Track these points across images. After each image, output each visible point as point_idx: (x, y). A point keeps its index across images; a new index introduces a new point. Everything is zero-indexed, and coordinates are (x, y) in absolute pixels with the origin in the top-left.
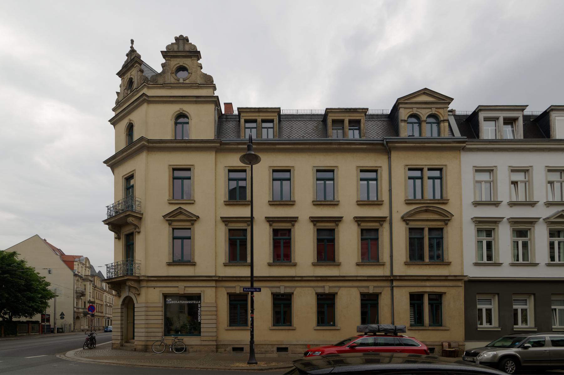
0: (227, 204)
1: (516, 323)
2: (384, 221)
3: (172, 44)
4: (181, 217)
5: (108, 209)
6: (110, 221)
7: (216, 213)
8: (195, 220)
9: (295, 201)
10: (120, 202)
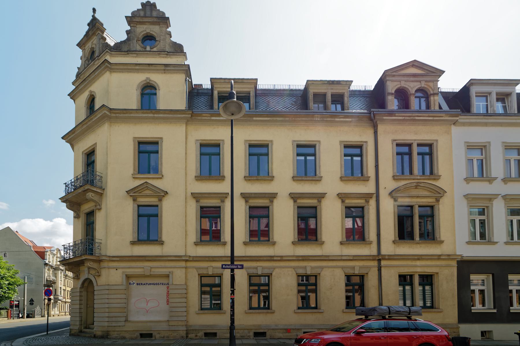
0: (199, 178)
1: (512, 305)
2: (371, 198)
3: (138, 10)
4: (148, 192)
5: (66, 186)
6: (67, 198)
7: (186, 189)
8: (163, 196)
10: (79, 177)
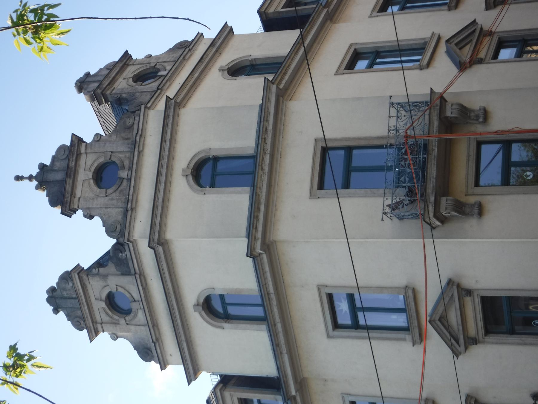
4: (454, 317)
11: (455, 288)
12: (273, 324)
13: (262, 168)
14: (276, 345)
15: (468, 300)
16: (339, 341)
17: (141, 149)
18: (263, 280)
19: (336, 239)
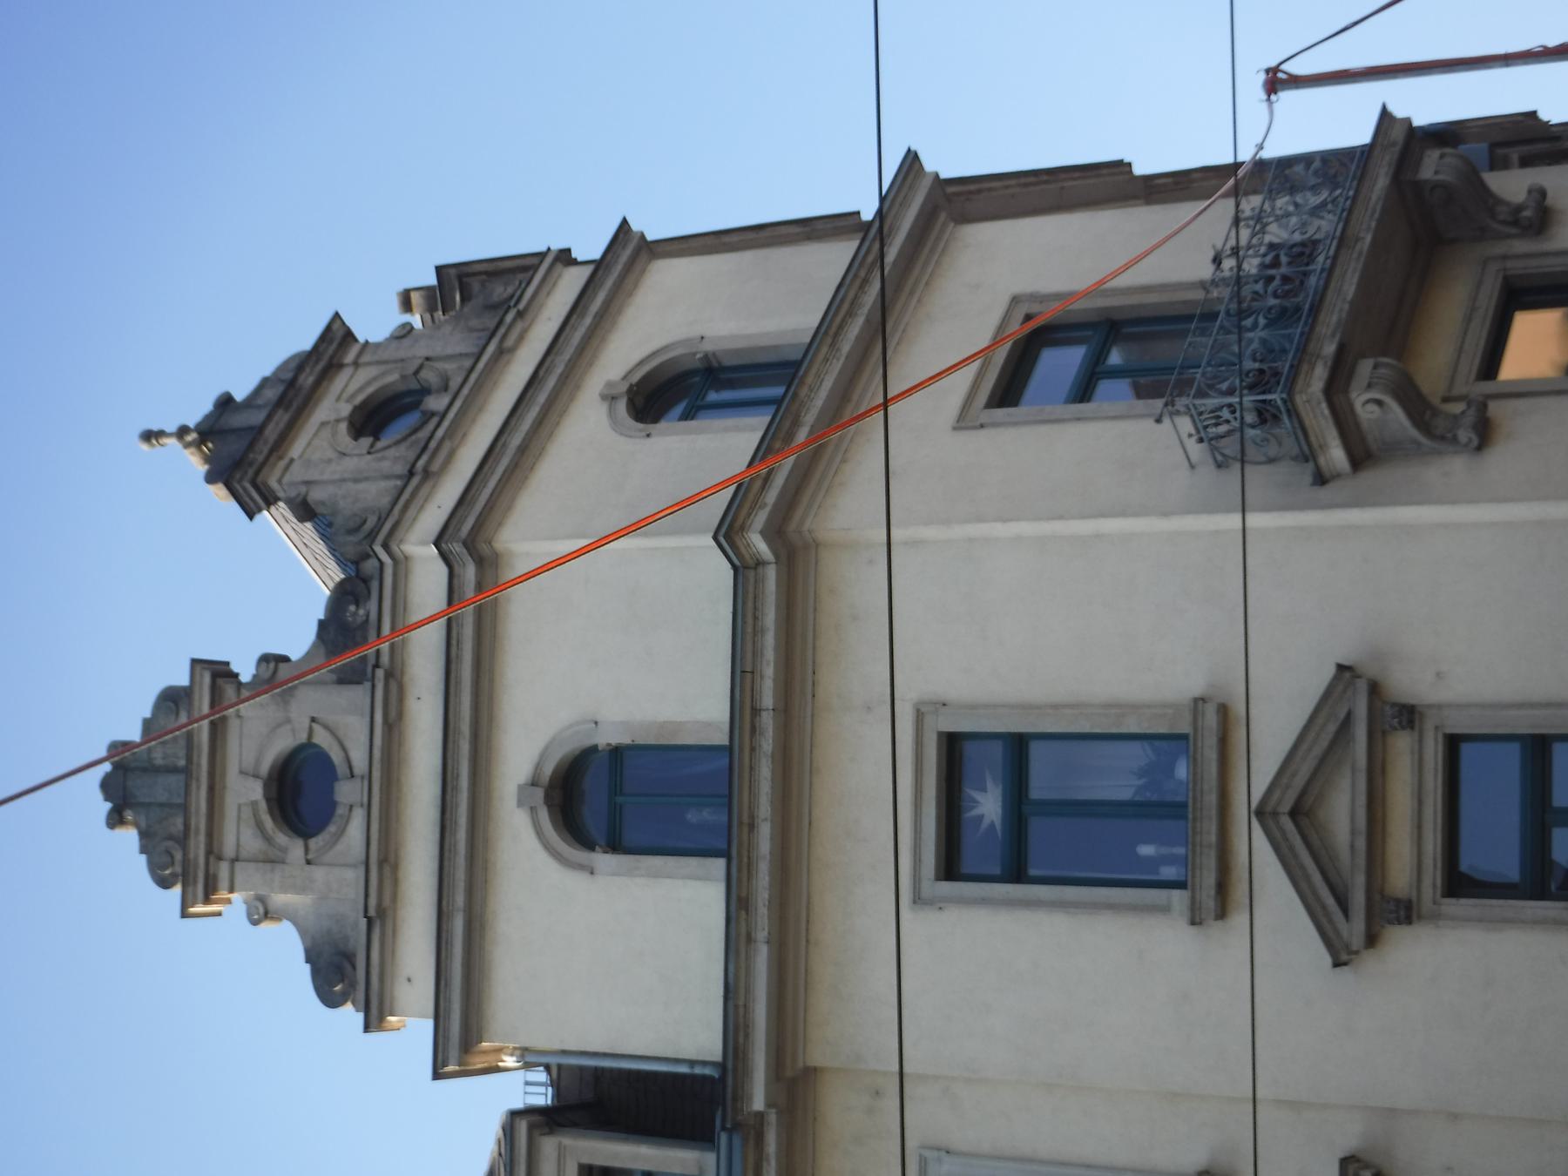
4: (1342, 811)
9: (1199, 701)
11: (1362, 686)
12: (745, 819)
13: (833, 345)
14: (740, 899)
15: (1402, 743)
16: (953, 917)
17: (509, 342)
18: (749, 655)
19: (1005, 520)
